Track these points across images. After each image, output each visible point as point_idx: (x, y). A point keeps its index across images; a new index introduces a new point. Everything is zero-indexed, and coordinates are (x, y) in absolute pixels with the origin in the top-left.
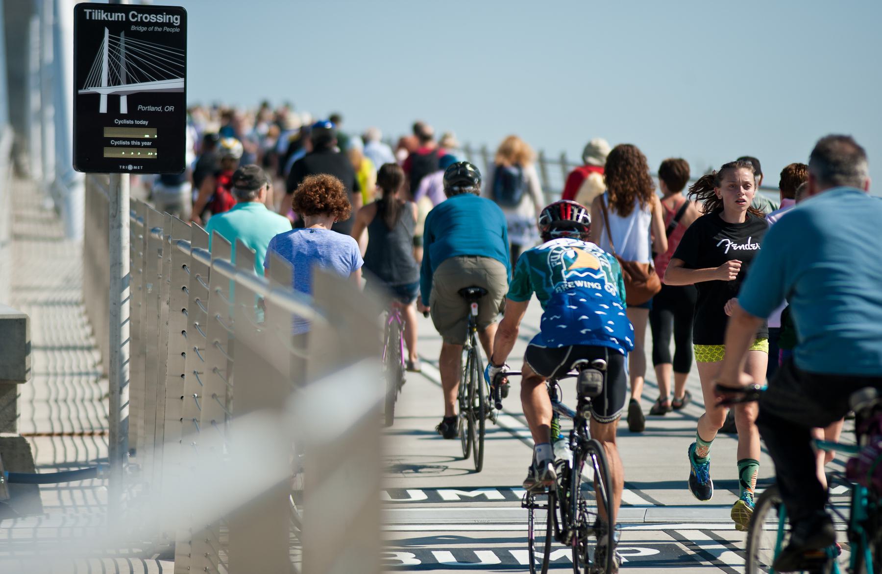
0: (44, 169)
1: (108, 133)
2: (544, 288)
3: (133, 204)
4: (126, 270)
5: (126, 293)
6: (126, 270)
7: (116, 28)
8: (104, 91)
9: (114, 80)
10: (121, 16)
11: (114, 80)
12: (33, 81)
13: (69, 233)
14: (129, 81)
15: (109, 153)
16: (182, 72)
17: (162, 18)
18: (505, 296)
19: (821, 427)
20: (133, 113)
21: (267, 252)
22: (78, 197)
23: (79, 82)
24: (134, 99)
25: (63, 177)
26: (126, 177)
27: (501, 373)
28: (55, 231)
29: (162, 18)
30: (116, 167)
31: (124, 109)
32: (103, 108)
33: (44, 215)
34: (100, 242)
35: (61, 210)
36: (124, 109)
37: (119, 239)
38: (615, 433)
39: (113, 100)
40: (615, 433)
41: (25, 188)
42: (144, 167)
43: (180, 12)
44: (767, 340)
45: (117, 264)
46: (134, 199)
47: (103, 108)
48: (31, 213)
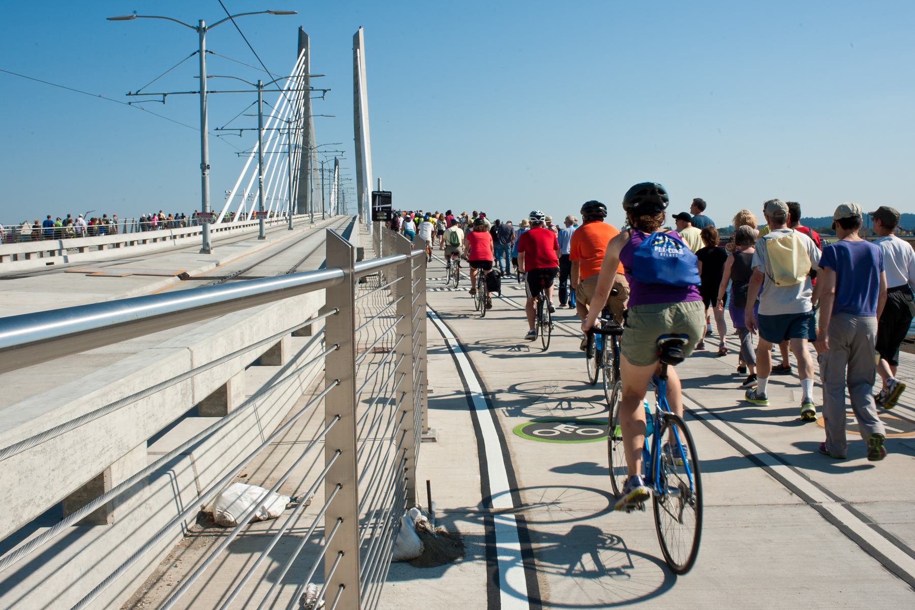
0: (365, 222)
1: (378, 214)
2: (893, 378)
3: (382, 227)
4: (381, 239)
5: (381, 243)
6: (381, 239)
7: (379, 195)
8: (377, 207)
9: (379, 205)
10: (379, 193)
11: (379, 205)
12: (363, 205)
13: (370, 234)
14: (382, 205)
15: (378, 218)
16: (390, 203)
17: (388, 194)
18: (812, 274)
19: (776, 343)
20: (382, 211)
21: (822, 253)
22: (372, 226)
23: (373, 205)
24: (382, 208)
25: (369, 223)
26: (381, 222)
27: (493, 228)
28: (367, 233)
29: (388, 194)
30: (379, 220)
31: (380, 210)
32: (377, 210)
33: (651, 243)
34: (376, 234)
35: (368, 229)
36: (380, 210)
37: (380, 233)
38: (520, 514)
39: (379, 208)
40: (520, 514)
41: (362, 225)
42: (384, 220)
43: (391, 192)
44: (801, 218)
45: (379, 237)
46: (813, 269)
47: (377, 210)
48: (363, 230)
